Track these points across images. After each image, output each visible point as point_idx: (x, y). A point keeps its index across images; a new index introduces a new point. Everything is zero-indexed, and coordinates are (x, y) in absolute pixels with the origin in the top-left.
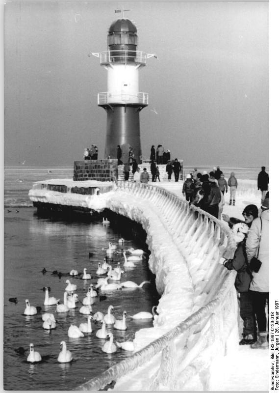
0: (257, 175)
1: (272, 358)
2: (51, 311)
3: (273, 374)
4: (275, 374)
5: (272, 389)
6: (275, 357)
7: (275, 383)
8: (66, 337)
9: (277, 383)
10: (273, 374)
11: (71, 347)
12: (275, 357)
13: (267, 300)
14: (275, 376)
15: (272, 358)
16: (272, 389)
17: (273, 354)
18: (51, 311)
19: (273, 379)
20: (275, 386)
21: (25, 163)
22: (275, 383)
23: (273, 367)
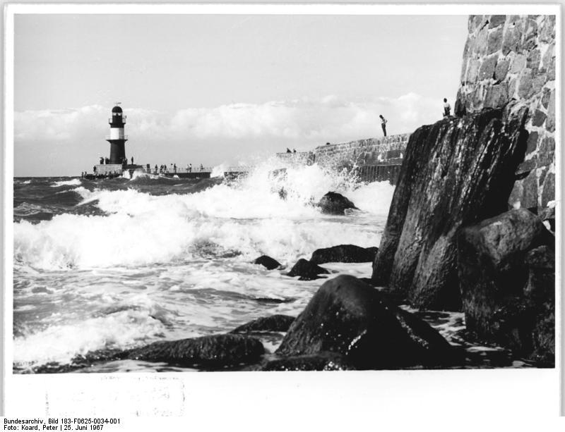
0: (372, 246)
1: (50, 421)
2: (50, 181)
3: (28, 422)
4: (27, 425)
5: (6, 421)
6: (52, 425)
7: (14, 425)
8: (544, 320)
9: (15, 428)
10: (28, 422)
11: (493, 310)
12: (52, 425)
13: (421, 367)
15: (50, 421)
16: (6, 421)
17: (57, 422)
18: (50, 181)
19: (20, 422)
20: (10, 425)
21: (534, 283)
22: (14, 425)
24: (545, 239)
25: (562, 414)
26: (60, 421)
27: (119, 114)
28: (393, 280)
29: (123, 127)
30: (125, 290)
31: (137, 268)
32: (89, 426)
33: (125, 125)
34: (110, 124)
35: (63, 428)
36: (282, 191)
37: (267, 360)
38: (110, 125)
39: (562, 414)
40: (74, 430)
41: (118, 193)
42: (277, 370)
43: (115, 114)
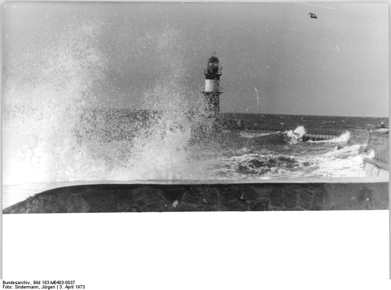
1: (35, 282)
3: (19, 283)
4: (19, 285)
5: (4, 282)
7: (9, 285)
9: (10, 287)
10: (19, 283)
12: (36, 285)
15: (35, 282)
16: (4, 282)
17: (39, 283)
19: (14, 283)
20: (7, 285)
22: (9, 285)
24: (389, 149)
25: (390, 279)
26: (41, 283)
27: (215, 65)
29: (218, 79)
33: (221, 77)
34: (206, 75)
35: (59, 287)
38: (205, 77)
39: (390, 279)
40: (64, 289)
41: (356, 157)
43: (211, 64)
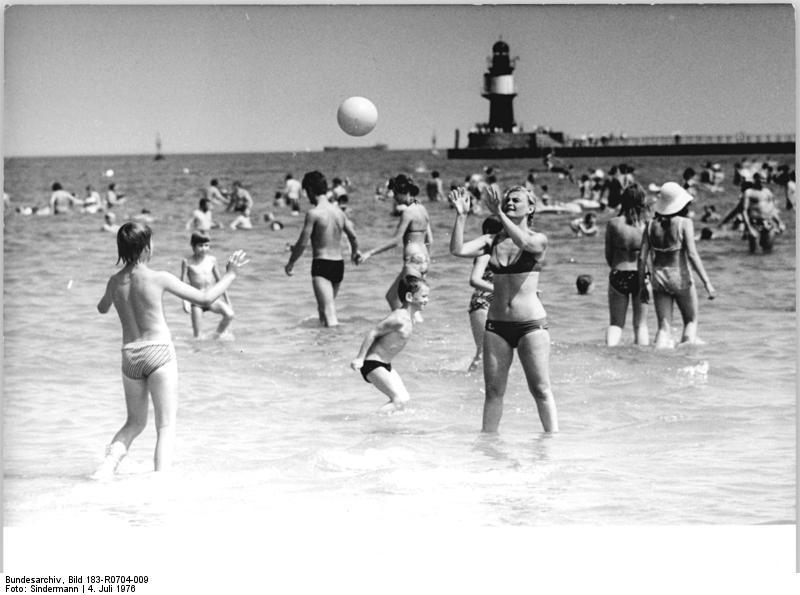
1: (71, 579)
3: (39, 581)
4: (39, 585)
5: (8, 579)
6: (73, 585)
7: (19, 585)
10: (39, 581)
12: (73, 585)
14: (35, 584)
15: (71, 579)
16: (8, 579)
19: (28, 580)
20: (14, 585)
22: (19, 585)
23: (54, 581)
25: (798, 571)
26: (85, 580)
28: (89, 200)
30: (421, 429)
31: (738, 329)
32: (114, 586)
36: (108, 454)
37: (423, 195)
39: (798, 571)
42: (289, 154)
